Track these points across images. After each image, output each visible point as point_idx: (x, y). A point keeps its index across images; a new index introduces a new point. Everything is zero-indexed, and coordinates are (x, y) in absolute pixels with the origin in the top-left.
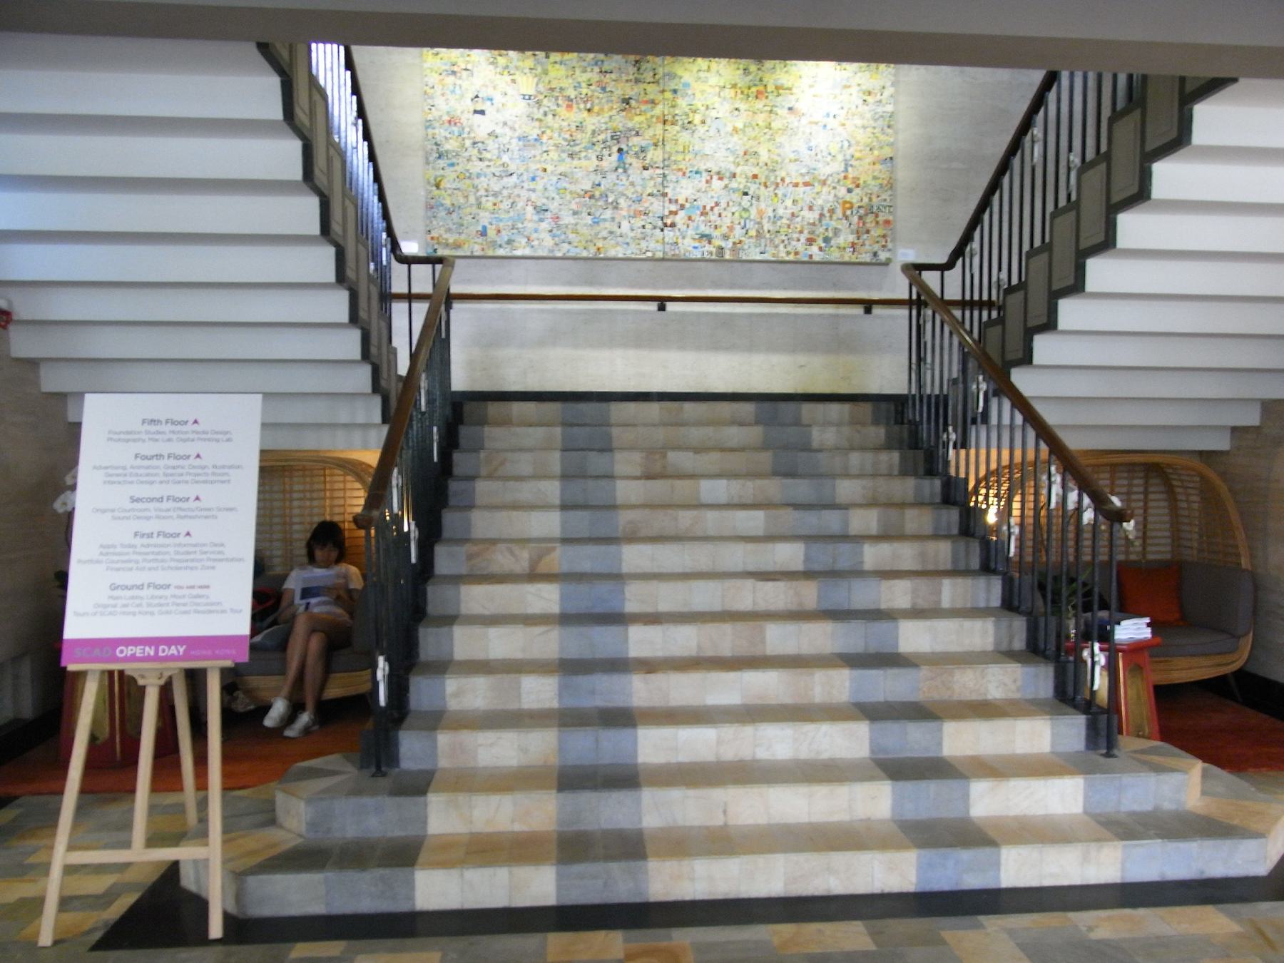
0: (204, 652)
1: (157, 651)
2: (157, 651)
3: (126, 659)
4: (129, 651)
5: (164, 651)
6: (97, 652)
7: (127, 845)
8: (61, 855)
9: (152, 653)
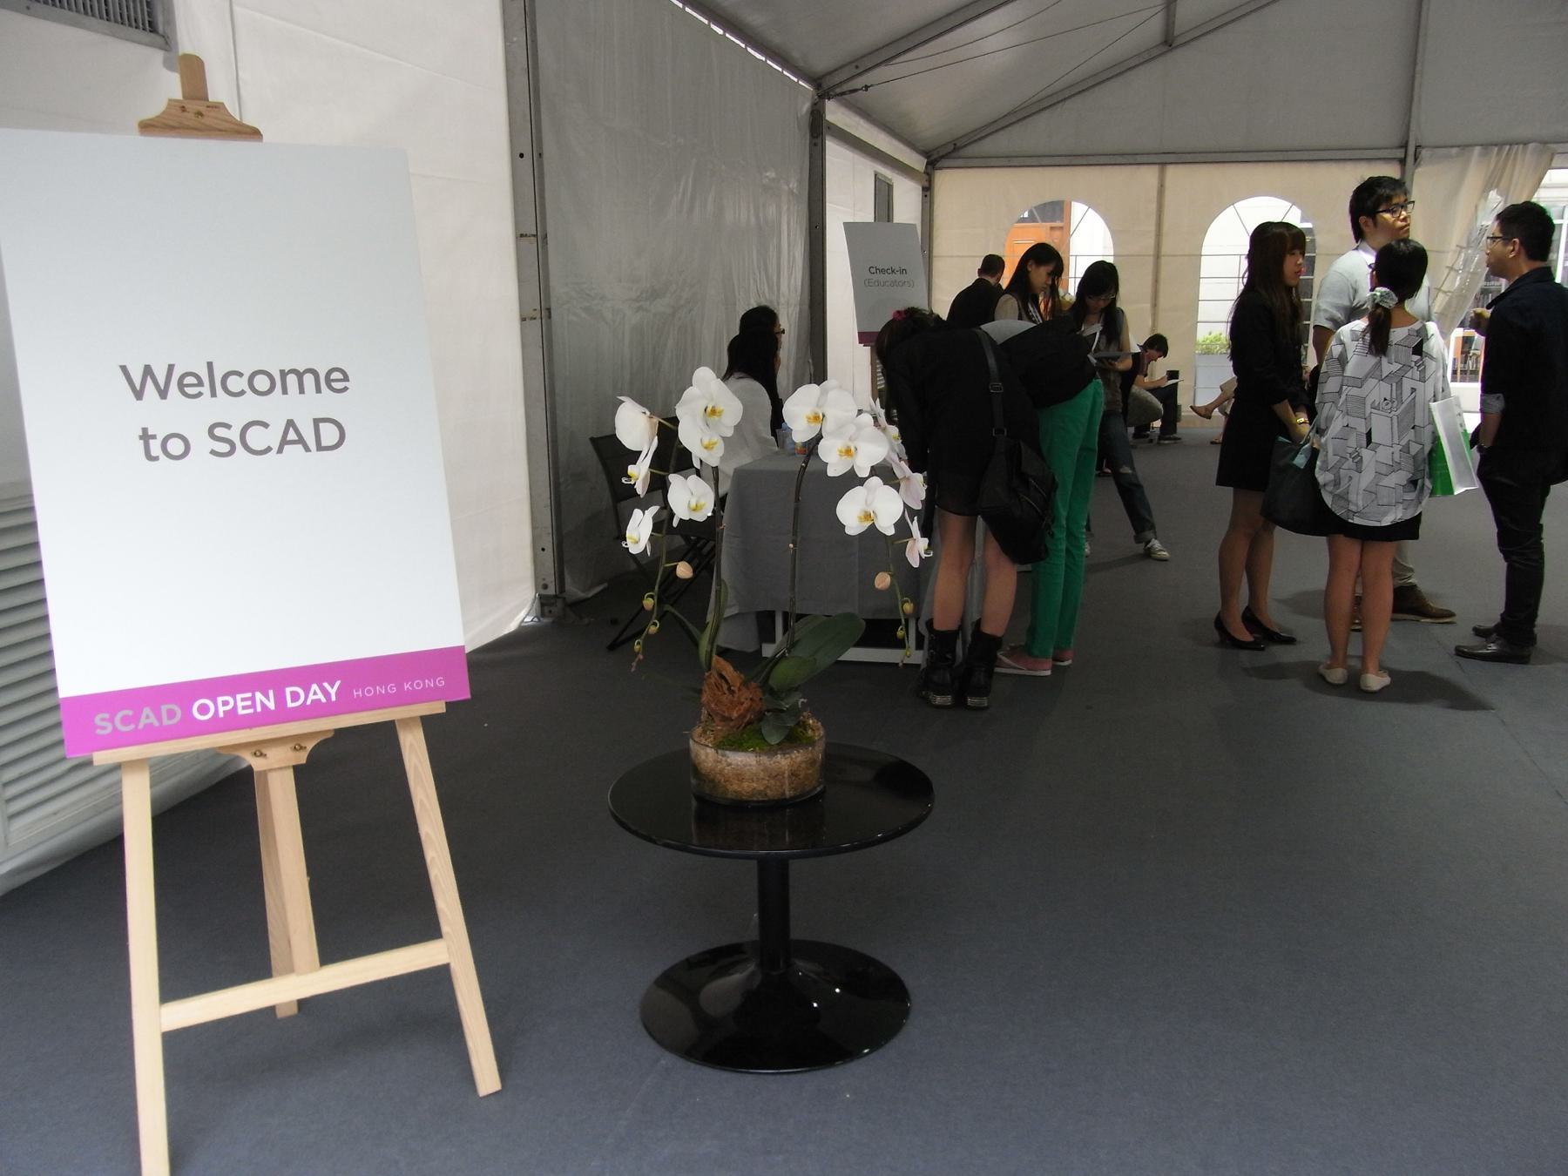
0: (381, 690)
1: (280, 699)
2: (280, 699)
3: (217, 725)
4: (222, 705)
5: (295, 696)
6: (147, 717)
7: (258, 967)
8: (154, 1018)
9: (271, 705)
